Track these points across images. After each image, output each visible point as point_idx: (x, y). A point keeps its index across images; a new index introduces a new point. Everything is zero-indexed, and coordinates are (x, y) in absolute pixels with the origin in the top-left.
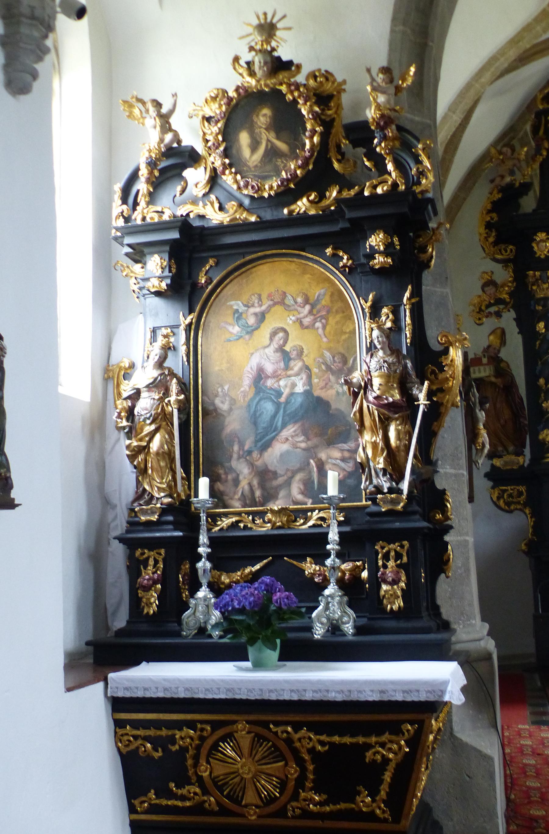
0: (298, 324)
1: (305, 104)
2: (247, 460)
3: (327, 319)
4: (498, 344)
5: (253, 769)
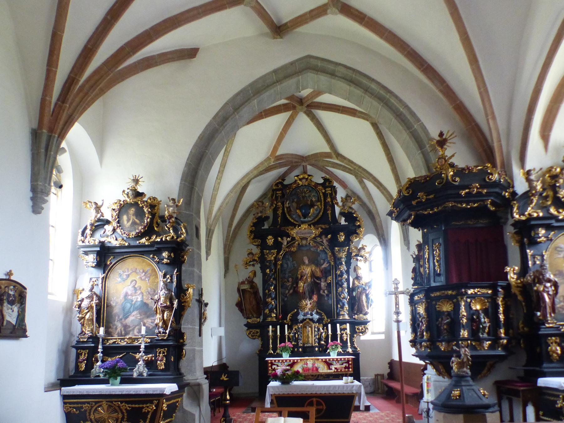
0: (140, 279)
1: (146, 208)
2: (120, 322)
3: (150, 278)
5: (108, 416)
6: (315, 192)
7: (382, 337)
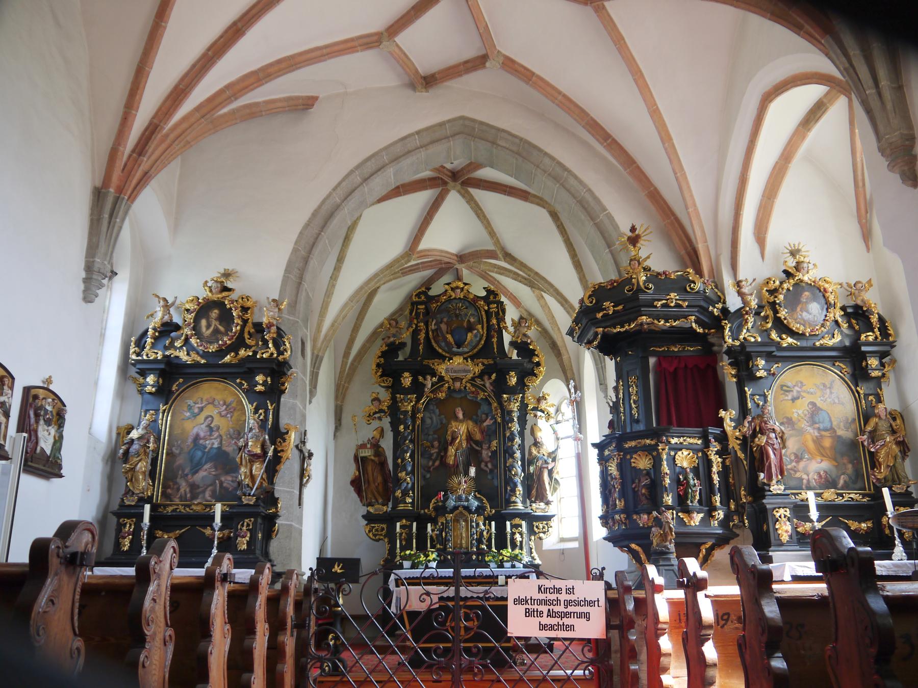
0: (218, 415)
4: (378, 437)
6: (474, 308)
7: (575, 545)
